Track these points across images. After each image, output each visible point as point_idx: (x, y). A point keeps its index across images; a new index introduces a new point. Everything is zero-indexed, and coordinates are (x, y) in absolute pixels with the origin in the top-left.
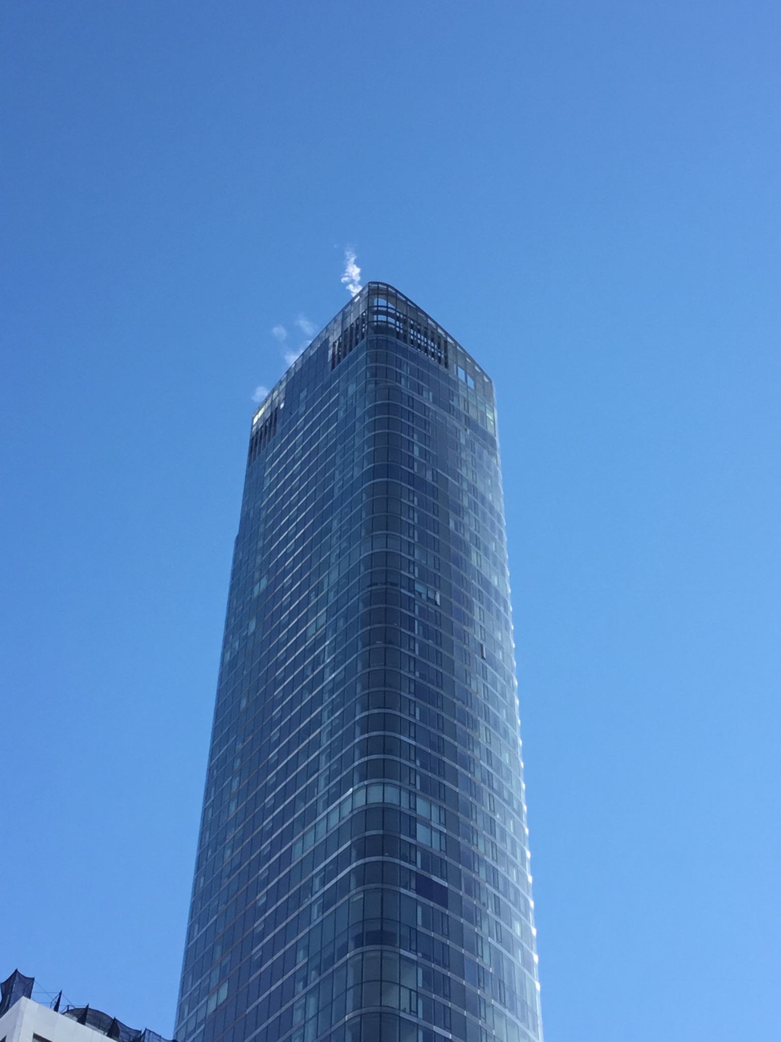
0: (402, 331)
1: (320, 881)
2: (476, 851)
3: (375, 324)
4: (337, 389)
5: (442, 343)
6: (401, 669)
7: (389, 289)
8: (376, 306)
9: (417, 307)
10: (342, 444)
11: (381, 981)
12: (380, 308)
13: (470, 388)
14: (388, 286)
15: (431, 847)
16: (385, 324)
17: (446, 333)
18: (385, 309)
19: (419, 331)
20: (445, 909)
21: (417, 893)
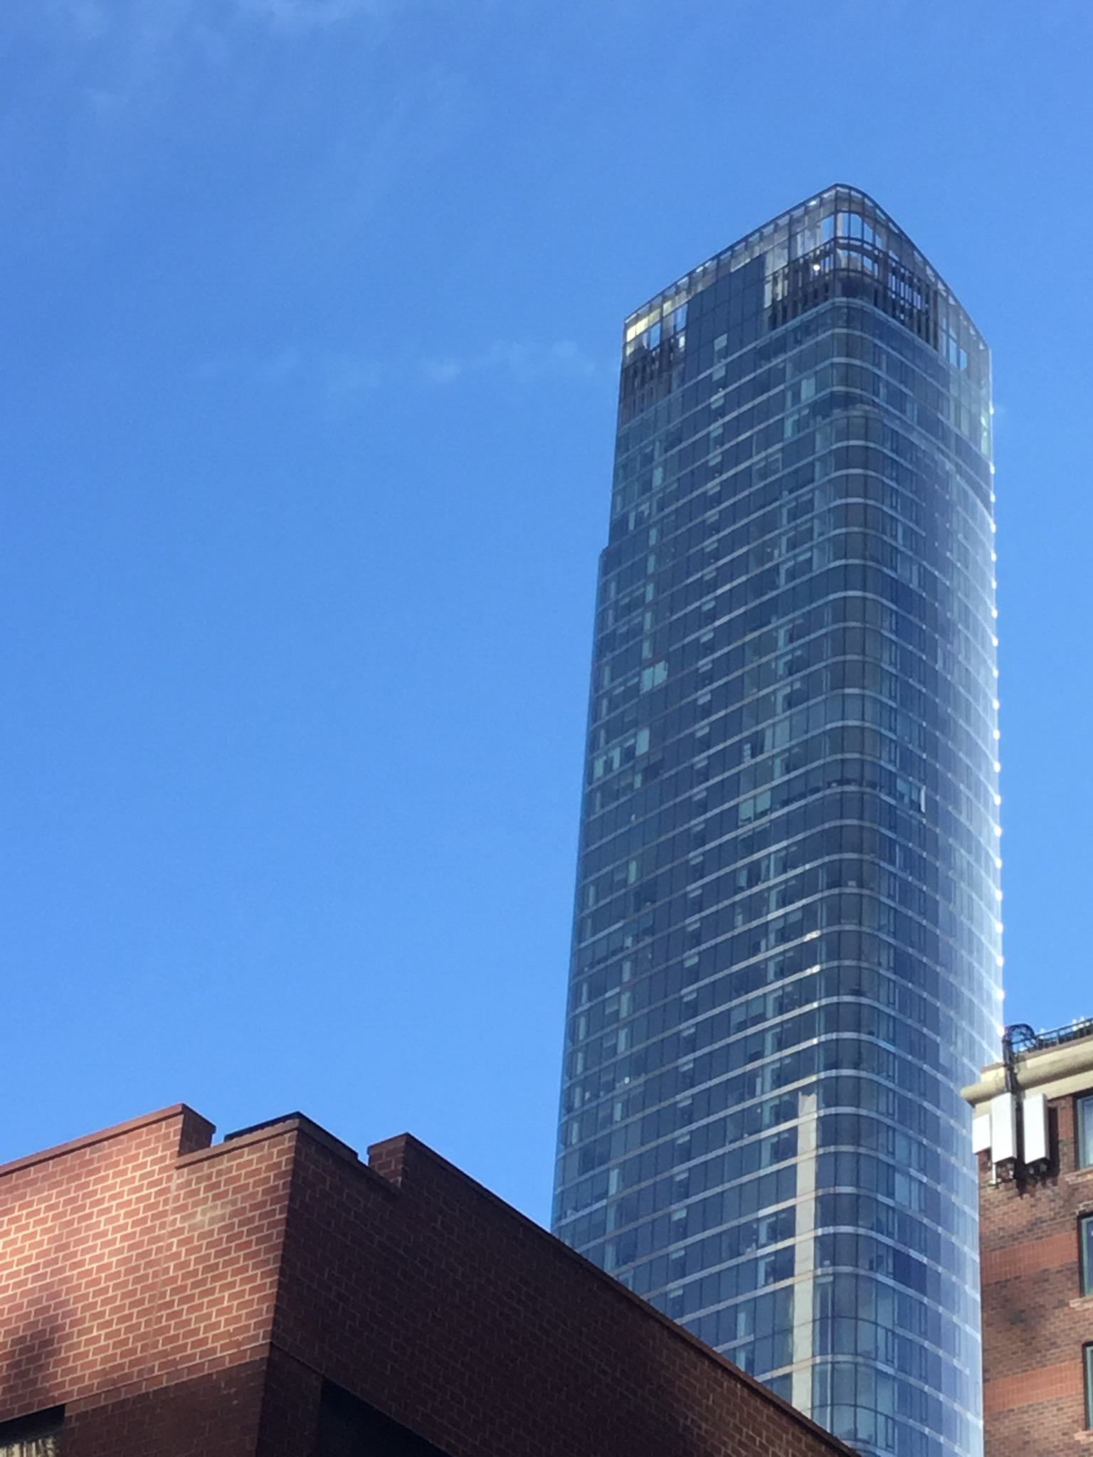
0: (881, 256)
1: (785, 635)
2: (959, 433)
3: (845, 273)
4: (778, 375)
5: (931, 294)
6: (879, 893)
7: (866, 200)
8: (844, 270)
9: (902, 232)
10: (791, 492)
11: (856, 1318)
12: (852, 242)
13: (955, 341)
14: (865, 195)
15: (910, 1208)
16: (859, 275)
17: (937, 276)
18: (858, 243)
19: (902, 278)
20: (921, 1296)
21: (894, 1279)
